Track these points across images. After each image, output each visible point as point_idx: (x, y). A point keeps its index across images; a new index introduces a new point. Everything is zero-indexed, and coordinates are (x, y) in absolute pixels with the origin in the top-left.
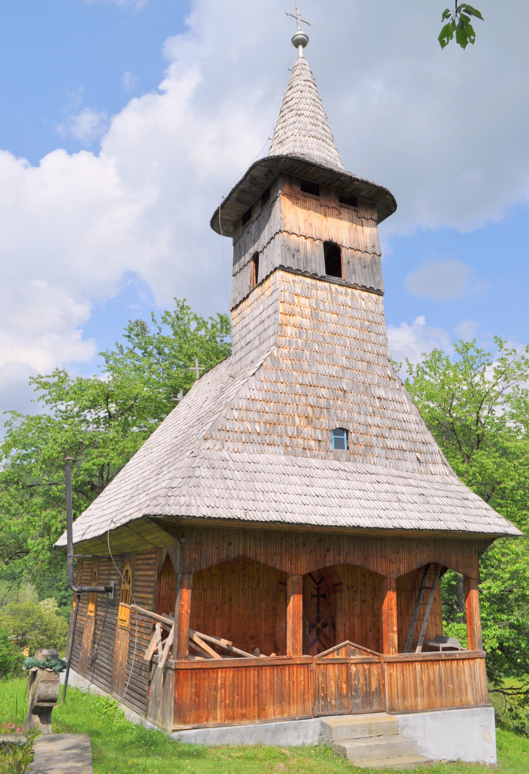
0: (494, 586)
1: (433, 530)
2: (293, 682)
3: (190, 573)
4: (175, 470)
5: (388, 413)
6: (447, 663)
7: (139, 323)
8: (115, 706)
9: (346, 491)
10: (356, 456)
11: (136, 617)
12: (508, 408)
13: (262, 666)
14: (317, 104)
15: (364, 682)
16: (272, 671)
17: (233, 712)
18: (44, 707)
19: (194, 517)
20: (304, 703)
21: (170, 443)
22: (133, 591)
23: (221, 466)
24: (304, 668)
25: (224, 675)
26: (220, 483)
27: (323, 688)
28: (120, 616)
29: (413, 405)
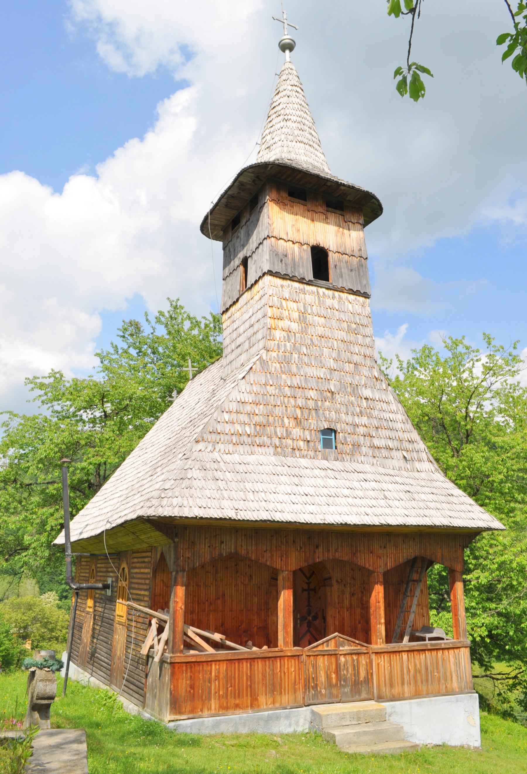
0: (482, 576)
1: (419, 525)
2: (285, 673)
3: (183, 570)
4: (168, 471)
5: (375, 413)
6: (433, 653)
7: (133, 323)
8: (113, 698)
9: (335, 490)
10: (344, 455)
11: (132, 613)
12: (496, 402)
13: (254, 658)
14: (304, 109)
15: (353, 672)
16: (264, 663)
17: (227, 702)
18: (43, 705)
19: (187, 517)
20: (295, 692)
21: (165, 443)
22: (130, 588)
23: (212, 468)
24: (295, 660)
25: (217, 667)
26: (212, 484)
27: (313, 678)
28: (117, 612)
29: (399, 405)
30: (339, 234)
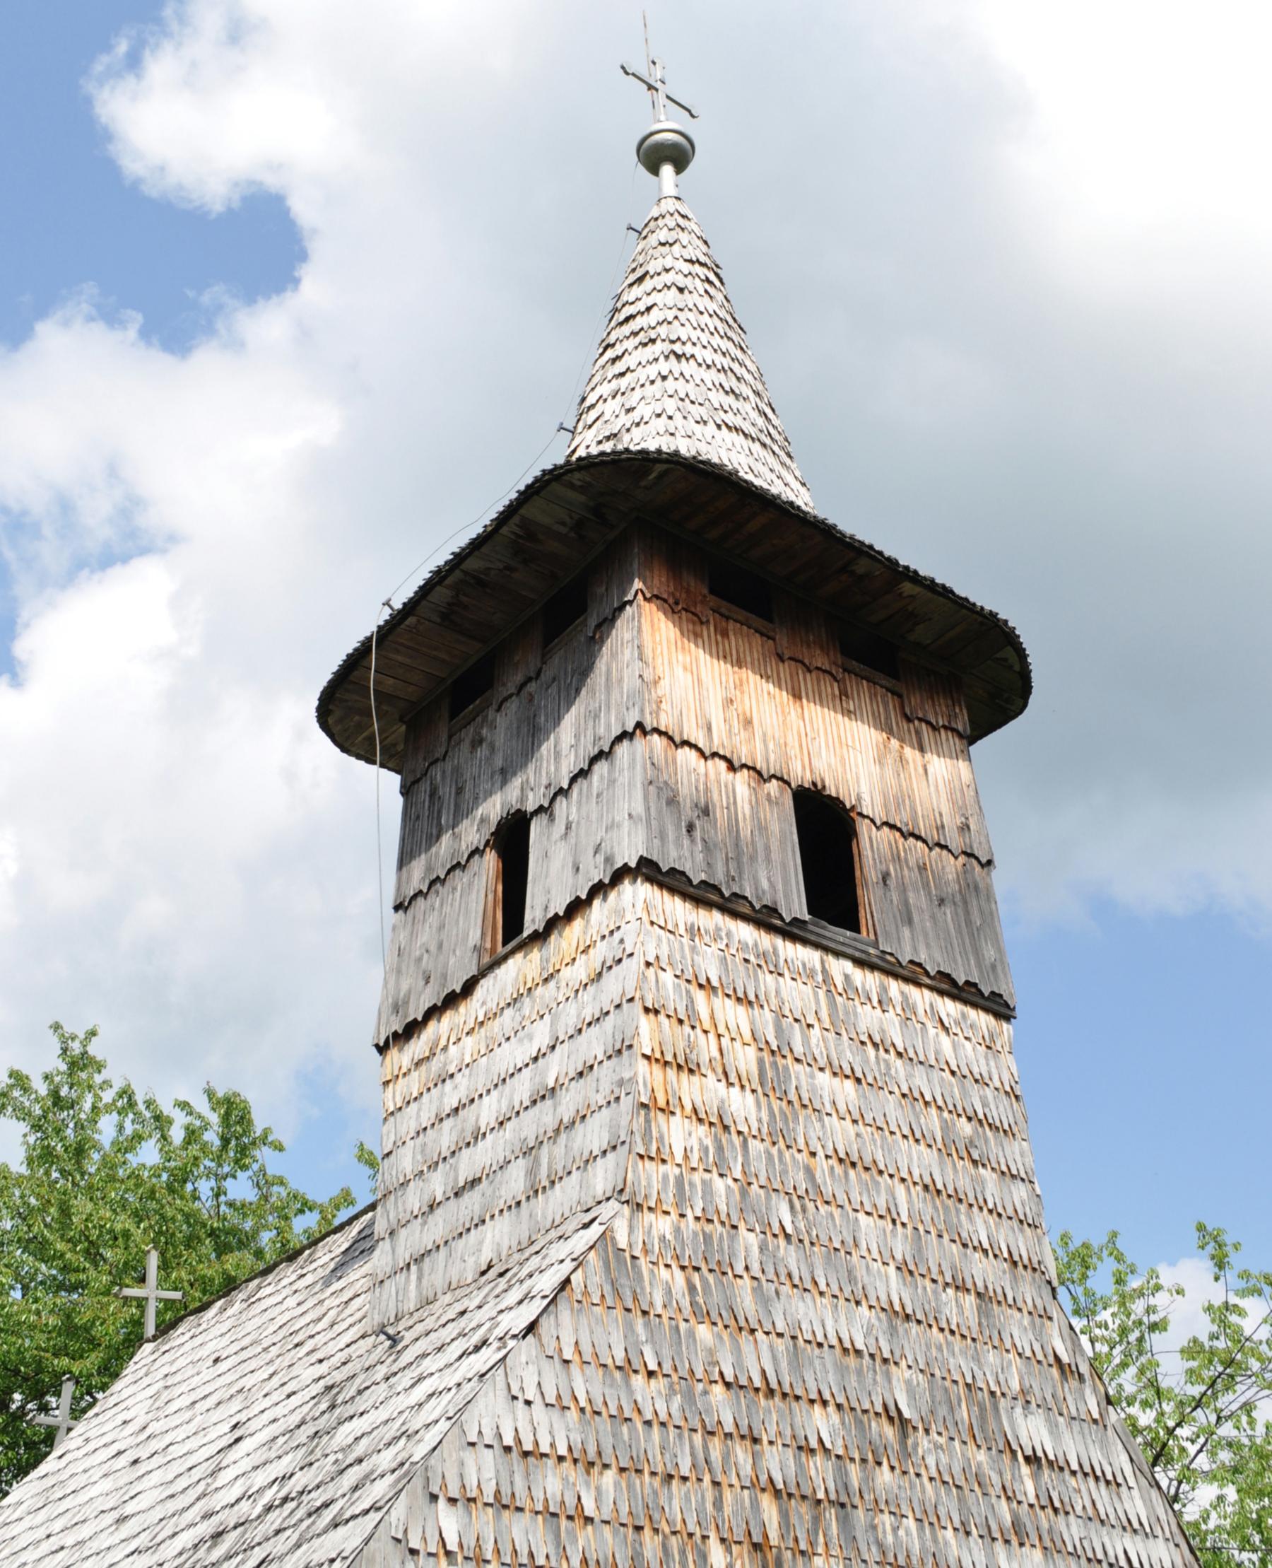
30: (889, 760)
